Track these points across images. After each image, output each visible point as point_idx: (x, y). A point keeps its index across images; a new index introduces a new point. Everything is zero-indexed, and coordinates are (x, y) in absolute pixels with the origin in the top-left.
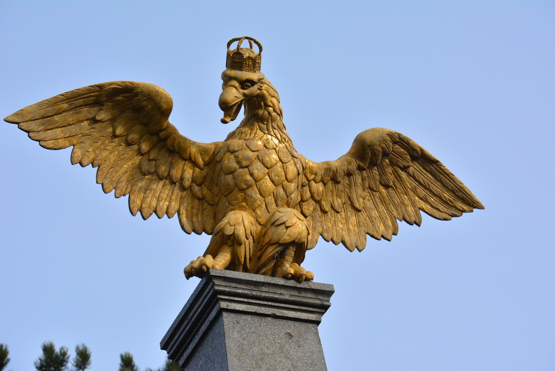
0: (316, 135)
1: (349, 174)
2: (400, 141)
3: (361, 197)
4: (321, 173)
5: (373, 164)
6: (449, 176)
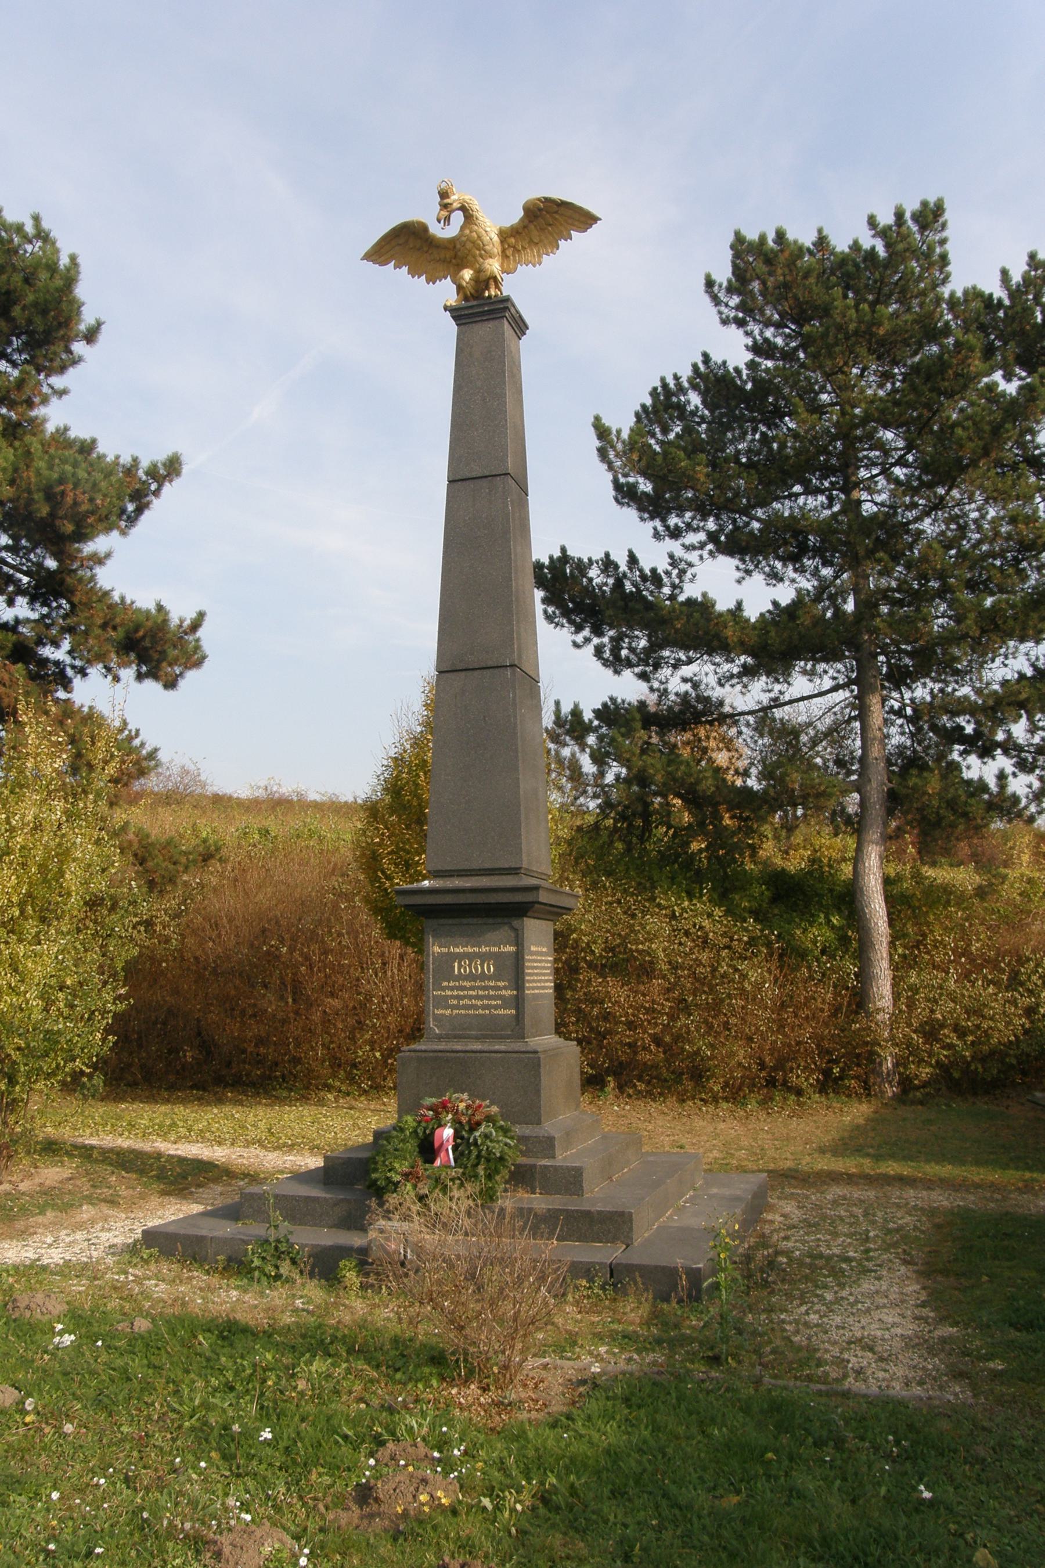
0: (497, 217)
1: (525, 227)
2: (547, 200)
3: (535, 234)
4: (526, 221)
5: (536, 217)
6: (581, 208)
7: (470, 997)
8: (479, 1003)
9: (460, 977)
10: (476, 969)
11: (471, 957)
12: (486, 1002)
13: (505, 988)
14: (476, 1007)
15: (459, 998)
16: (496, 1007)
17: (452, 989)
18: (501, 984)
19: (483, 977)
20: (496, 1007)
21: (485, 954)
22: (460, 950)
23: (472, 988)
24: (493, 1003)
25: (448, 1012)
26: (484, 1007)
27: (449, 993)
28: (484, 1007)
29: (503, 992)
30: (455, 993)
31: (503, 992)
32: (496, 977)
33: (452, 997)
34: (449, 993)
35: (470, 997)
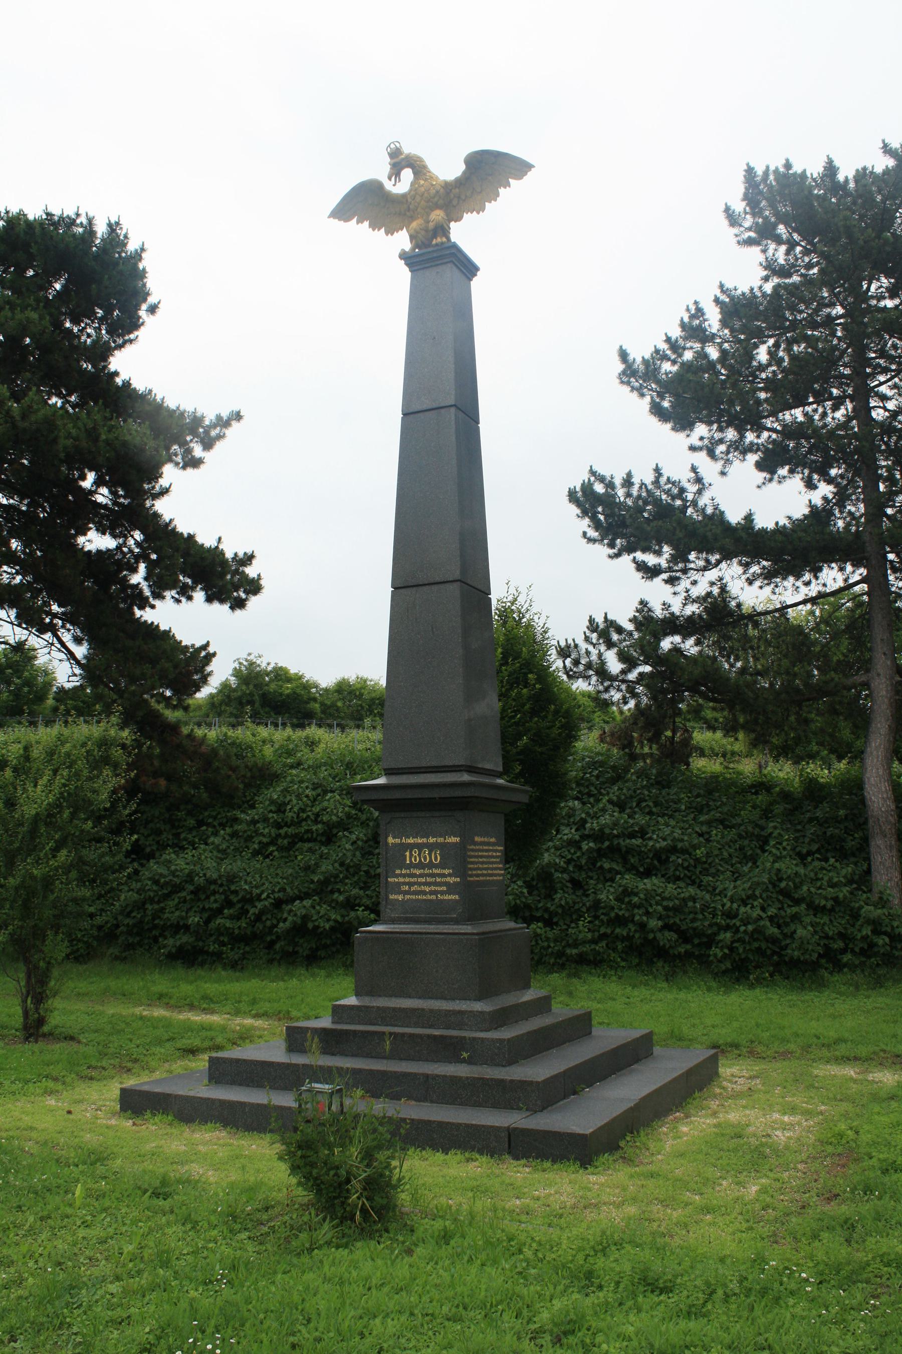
7: (420, 884)
8: (427, 889)
9: (411, 866)
10: (425, 858)
11: (420, 847)
12: (433, 888)
13: (450, 875)
14: (424, 893)
15: (410, 884)
16: (442, 893)
17: (404, 876)
18: (446, 872)
19: (431, 865)
20: (442, 893)
21: (432, 844)
22: (411, 841)
23: (421, 876)
24: (440, 889)
25: (400, 897)
26: (431, 893)
27: (401, 880)
28: (431, 893)
29: (448, 879)
30: (407, 880)
31: (448, 879)
32: (442, 866)
33: (405, 883)
34: (401, 880)
35: (420, 884)
